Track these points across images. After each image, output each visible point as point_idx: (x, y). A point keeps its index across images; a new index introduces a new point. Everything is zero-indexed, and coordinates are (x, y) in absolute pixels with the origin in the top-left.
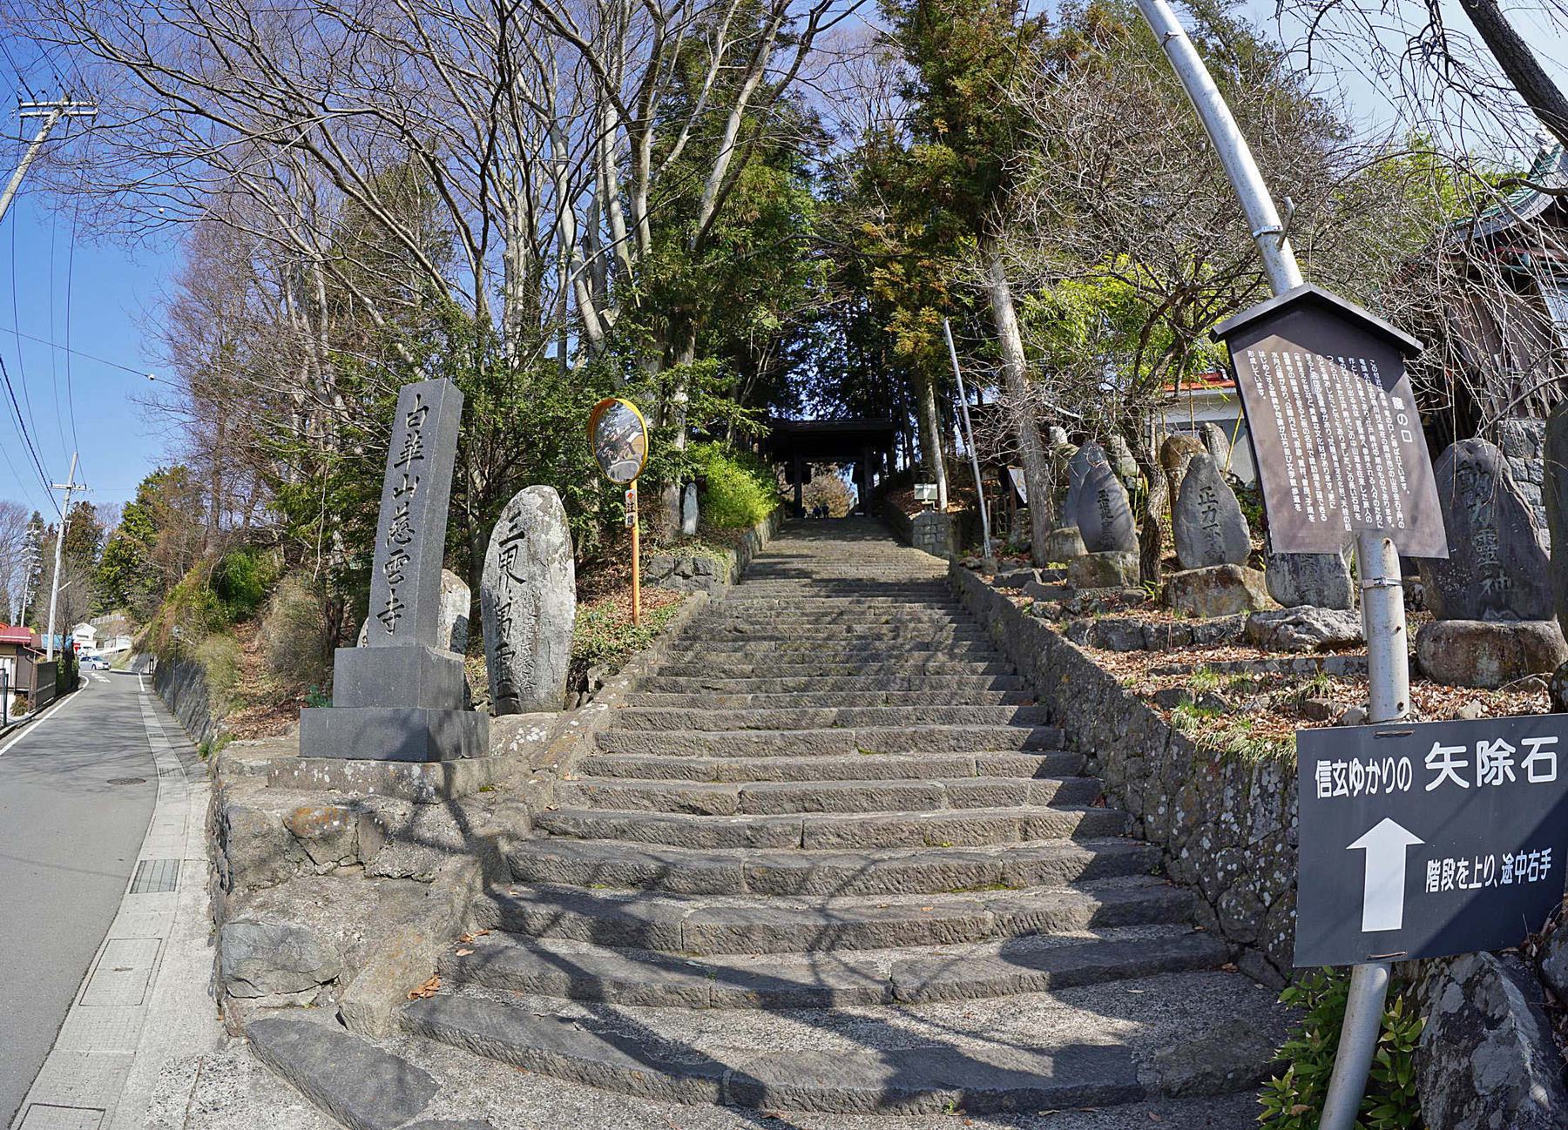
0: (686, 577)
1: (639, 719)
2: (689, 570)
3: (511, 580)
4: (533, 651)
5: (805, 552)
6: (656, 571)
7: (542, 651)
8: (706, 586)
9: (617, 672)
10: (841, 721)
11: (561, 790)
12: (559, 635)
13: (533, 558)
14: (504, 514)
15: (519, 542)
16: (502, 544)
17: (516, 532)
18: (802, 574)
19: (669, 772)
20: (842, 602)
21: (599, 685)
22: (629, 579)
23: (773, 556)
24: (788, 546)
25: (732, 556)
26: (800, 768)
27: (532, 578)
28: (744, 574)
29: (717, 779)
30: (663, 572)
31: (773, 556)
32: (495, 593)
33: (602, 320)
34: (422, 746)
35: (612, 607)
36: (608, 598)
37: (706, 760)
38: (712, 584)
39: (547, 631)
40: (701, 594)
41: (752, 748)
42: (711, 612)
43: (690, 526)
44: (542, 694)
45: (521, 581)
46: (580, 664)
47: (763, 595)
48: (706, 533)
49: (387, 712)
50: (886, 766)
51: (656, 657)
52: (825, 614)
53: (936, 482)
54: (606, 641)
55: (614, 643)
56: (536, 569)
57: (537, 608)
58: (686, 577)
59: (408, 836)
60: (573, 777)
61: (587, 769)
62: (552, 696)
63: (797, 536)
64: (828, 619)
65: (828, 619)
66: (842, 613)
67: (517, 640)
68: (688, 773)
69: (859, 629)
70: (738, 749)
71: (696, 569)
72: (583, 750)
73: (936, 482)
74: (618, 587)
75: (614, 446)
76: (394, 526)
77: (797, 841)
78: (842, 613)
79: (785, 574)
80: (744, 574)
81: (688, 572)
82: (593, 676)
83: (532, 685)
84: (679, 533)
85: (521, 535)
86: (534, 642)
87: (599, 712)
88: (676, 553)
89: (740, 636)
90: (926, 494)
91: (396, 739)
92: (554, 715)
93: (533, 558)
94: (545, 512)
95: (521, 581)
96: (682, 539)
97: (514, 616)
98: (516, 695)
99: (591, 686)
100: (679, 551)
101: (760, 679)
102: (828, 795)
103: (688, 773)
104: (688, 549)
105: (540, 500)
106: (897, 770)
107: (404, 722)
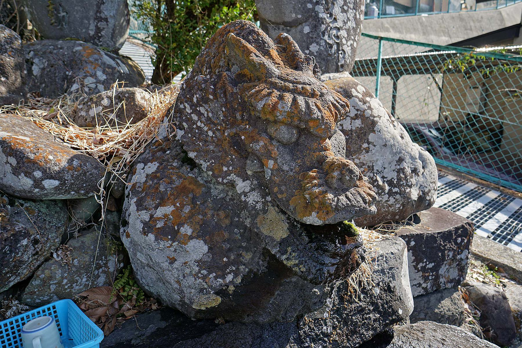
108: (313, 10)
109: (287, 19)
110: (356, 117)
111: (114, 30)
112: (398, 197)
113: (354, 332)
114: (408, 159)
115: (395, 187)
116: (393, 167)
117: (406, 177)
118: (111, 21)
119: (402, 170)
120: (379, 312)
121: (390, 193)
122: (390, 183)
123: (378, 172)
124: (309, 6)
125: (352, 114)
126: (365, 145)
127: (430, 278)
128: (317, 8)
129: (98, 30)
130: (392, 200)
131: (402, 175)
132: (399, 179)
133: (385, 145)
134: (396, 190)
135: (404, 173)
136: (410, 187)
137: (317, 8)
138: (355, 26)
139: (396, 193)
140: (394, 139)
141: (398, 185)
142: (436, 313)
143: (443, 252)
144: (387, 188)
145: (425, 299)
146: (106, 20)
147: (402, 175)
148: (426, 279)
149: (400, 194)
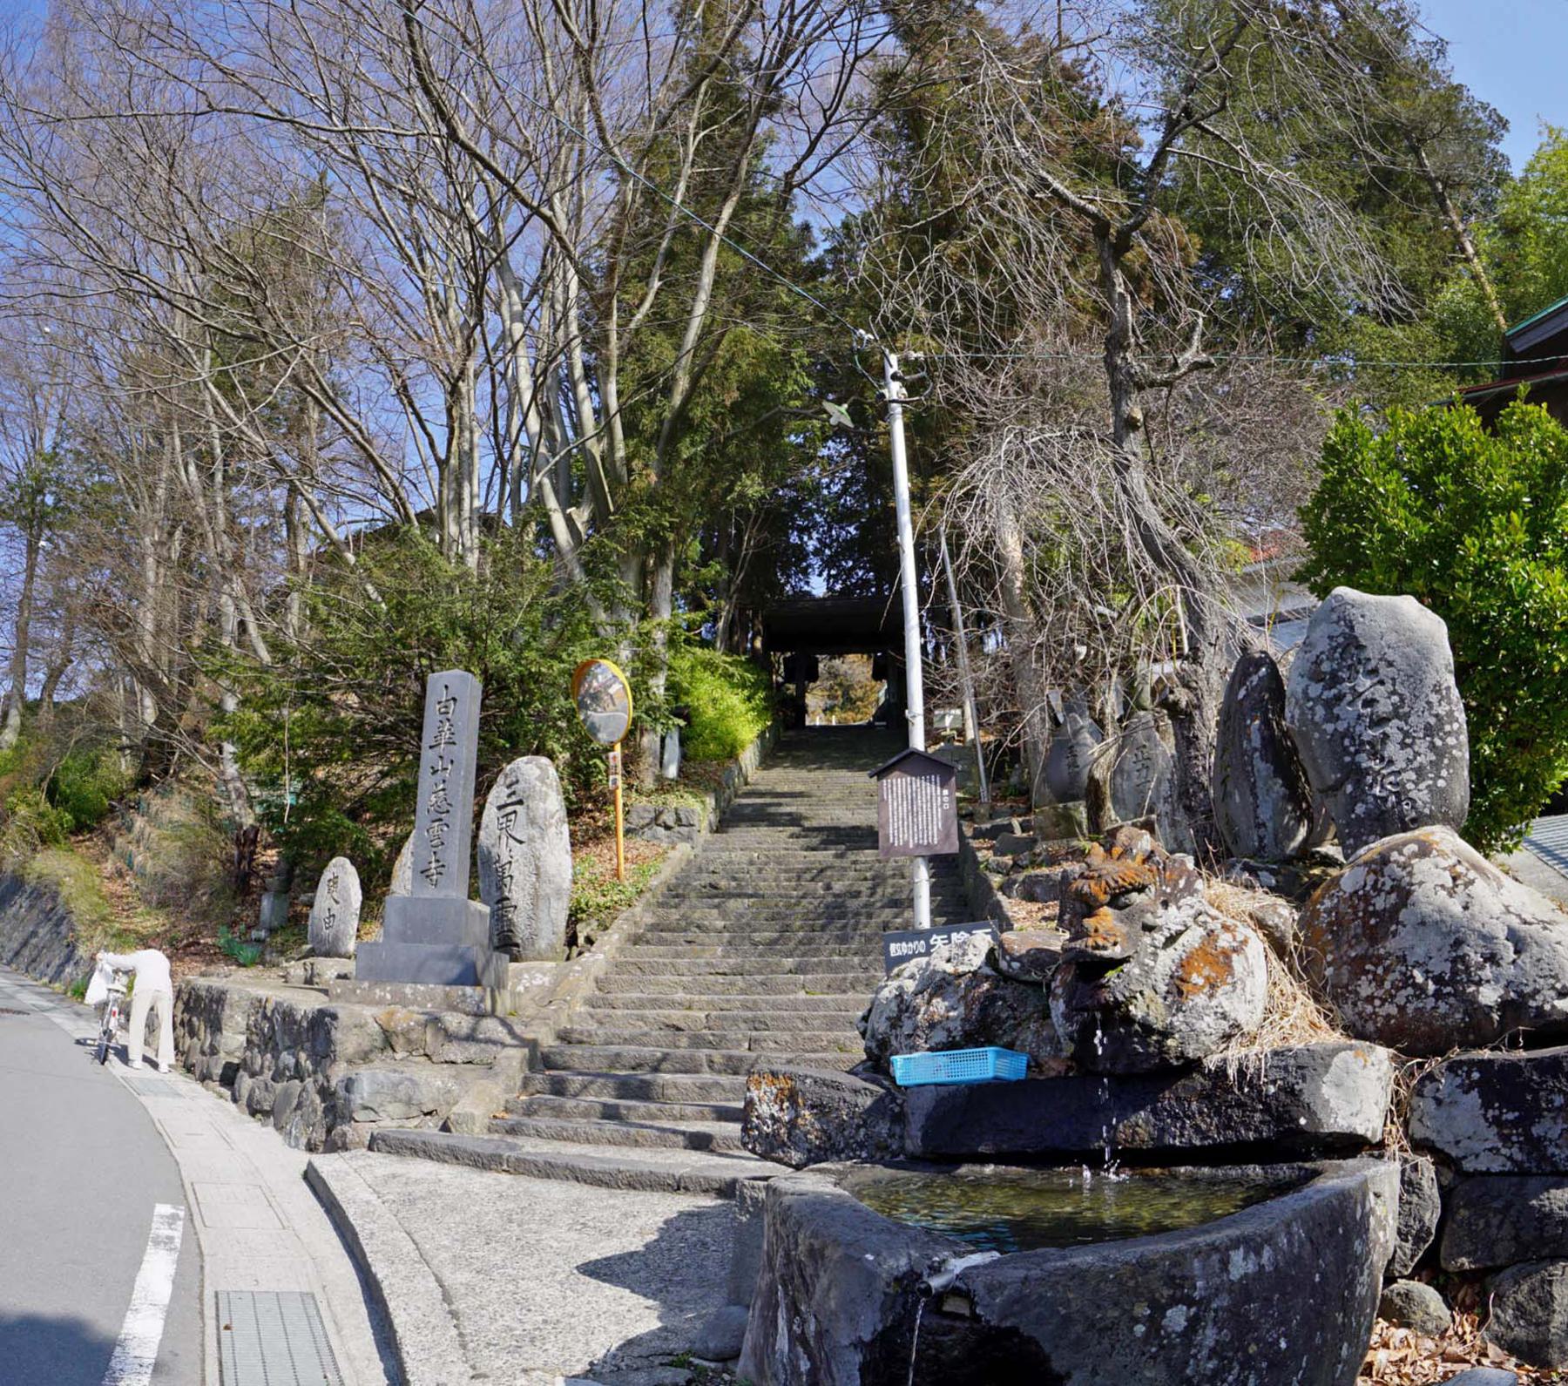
0: (668, 828)
1: (630, 968)
2: (670, 821)
3: (511, 841)
4: (535, 905)
5: (799, 788)
6: (635, 821)
7: (542, 905)
8: (689, 838)
9: (606, 928)
10: (799, 969)
11: (576, 1014)
12: (558, 892)
13: (532, 822)
14: (501, 779)
15: (518, 808)
16: (500, 808)
17: (514, 799)
18: (794, 820)
19: (655, 1003)
20: (826, 856)
21: (589, 941)
22: (608, 830)
23: (762, 795)
24: (785, 778)
25: (710, 801)
26: (755, 1002)
27: (532, 840)
28: (728, 819)
29: (689, 1008)
30: (643, 822)
31: (762, 795)
32: (494, 851)
33: (569, 520)
34: (470, 976)
35: (599, 859)
36: (585, 850)
37: (680, 995)
38: (695, 836)
39: (546, 889)
40: (684, 847)
41: (719, 988)
42: (692, 867)
43: (672, 771)
44: (542, 944)
45: (521, 842)
46: (573, 919)
47: (753, 845)
48: (689, 778)
49: (442, 948)
50: (823, 1001)
51: (643, 915)
52: (808, 870)
53: (961, 707)
54: (594, 898)
55: (601, 900)
56: (535, 832)
57: (537, 868)
58: (668, 828)
59: (471, 1038)
60: (581, 1008)
61: (591, 1003)
62: (552, 947)
63: (798, 763)
64: (808, 876)
65: (808, 876)
66: (822, 871)
67: (518, 893)
68: (673, 1004)
69: (838, 887)
70: (708, 989)
71: (679, 820)
72: (588, 989)
73: (961, 707)
74: (596, 839)
75: (595, 697)
76: (433, 799)
77: (746, 1045)
78: (822, 871)
79: (773, 820)
80: (728, 819)
81: (671, 822)
82: (583, 932)
83: (533, 936)
84: (660, 779)
85: (520, 802)
86: (536, 898)
87: (597, 960)
88: (658, 800)
89: (714, 892)
90: (948, 721)
91: (455, 969)
92: (553, 964)
93: (532, 822)
94: (543, 782)
95: (521, 842)
96: (663, 786)
97: (516, 874)
98: (517, 945)
99: (581, 940)
100: (661, 800)
101: (738, 934)
102: (773, 1019)
103: (673, 1004)
104: (671, 798)
105: (538, 772)
106: (831, 1004)
107: (461, 958)
108: (1353, 762)
109: (1331, 783)
110: (1393, 889)
111: (1276, 836)
112: (1452, 1000)
113: (1228, 1127)
114: (1472, 939)
115: (1447, 984)
116: (1446, 955)
117: (1468, 968)
118: (1270, 825)
119: (1463, 959)
120: (1271, 1115)
121: (1438, 995)
122: (1438, 980)
123: (1417, 965)
124: (1347, 759)
125: (1387, 888)
126: (1393, 928)
127: (1514, 1139)
128: (1358, 758)
129: (1261, 839)
130: (1443, 1008)
131: (1460, 966)
132: (1454, 973)
133: (1423, 923)
134: (1449, 989)
135: (1464, 962)
136: (1479, 983)
137: (1358, 758)
138: (1434, 758)
139: (1449, 994)
140: (1440, 912)
141: (1453, 982)
142: (1532, 1207)
143: (1535, 1092)
144: (1431, 987)
145: (1515, 1180)
146: (1264, 825)
147: (1460, 966)
148: (1505, 1139)
149: (1454, 995)
